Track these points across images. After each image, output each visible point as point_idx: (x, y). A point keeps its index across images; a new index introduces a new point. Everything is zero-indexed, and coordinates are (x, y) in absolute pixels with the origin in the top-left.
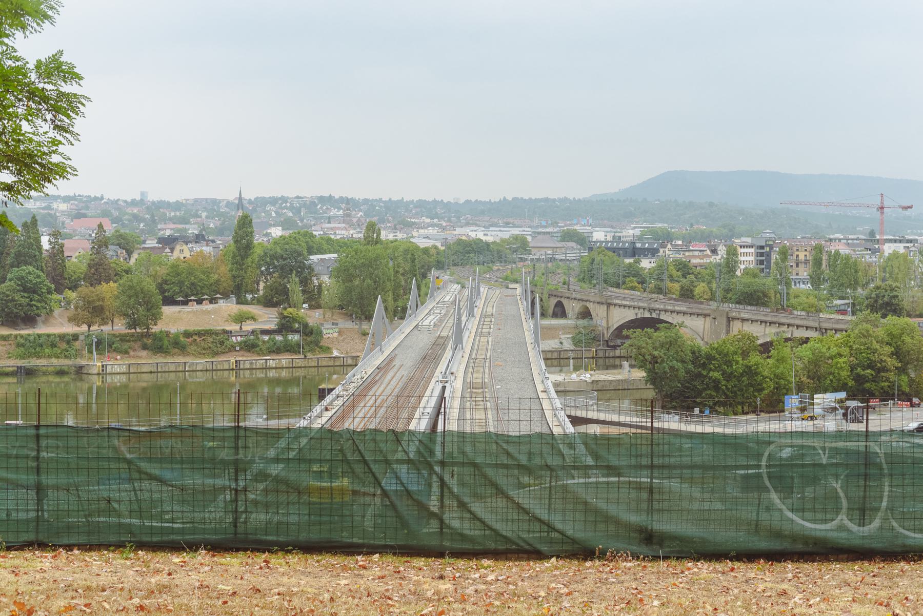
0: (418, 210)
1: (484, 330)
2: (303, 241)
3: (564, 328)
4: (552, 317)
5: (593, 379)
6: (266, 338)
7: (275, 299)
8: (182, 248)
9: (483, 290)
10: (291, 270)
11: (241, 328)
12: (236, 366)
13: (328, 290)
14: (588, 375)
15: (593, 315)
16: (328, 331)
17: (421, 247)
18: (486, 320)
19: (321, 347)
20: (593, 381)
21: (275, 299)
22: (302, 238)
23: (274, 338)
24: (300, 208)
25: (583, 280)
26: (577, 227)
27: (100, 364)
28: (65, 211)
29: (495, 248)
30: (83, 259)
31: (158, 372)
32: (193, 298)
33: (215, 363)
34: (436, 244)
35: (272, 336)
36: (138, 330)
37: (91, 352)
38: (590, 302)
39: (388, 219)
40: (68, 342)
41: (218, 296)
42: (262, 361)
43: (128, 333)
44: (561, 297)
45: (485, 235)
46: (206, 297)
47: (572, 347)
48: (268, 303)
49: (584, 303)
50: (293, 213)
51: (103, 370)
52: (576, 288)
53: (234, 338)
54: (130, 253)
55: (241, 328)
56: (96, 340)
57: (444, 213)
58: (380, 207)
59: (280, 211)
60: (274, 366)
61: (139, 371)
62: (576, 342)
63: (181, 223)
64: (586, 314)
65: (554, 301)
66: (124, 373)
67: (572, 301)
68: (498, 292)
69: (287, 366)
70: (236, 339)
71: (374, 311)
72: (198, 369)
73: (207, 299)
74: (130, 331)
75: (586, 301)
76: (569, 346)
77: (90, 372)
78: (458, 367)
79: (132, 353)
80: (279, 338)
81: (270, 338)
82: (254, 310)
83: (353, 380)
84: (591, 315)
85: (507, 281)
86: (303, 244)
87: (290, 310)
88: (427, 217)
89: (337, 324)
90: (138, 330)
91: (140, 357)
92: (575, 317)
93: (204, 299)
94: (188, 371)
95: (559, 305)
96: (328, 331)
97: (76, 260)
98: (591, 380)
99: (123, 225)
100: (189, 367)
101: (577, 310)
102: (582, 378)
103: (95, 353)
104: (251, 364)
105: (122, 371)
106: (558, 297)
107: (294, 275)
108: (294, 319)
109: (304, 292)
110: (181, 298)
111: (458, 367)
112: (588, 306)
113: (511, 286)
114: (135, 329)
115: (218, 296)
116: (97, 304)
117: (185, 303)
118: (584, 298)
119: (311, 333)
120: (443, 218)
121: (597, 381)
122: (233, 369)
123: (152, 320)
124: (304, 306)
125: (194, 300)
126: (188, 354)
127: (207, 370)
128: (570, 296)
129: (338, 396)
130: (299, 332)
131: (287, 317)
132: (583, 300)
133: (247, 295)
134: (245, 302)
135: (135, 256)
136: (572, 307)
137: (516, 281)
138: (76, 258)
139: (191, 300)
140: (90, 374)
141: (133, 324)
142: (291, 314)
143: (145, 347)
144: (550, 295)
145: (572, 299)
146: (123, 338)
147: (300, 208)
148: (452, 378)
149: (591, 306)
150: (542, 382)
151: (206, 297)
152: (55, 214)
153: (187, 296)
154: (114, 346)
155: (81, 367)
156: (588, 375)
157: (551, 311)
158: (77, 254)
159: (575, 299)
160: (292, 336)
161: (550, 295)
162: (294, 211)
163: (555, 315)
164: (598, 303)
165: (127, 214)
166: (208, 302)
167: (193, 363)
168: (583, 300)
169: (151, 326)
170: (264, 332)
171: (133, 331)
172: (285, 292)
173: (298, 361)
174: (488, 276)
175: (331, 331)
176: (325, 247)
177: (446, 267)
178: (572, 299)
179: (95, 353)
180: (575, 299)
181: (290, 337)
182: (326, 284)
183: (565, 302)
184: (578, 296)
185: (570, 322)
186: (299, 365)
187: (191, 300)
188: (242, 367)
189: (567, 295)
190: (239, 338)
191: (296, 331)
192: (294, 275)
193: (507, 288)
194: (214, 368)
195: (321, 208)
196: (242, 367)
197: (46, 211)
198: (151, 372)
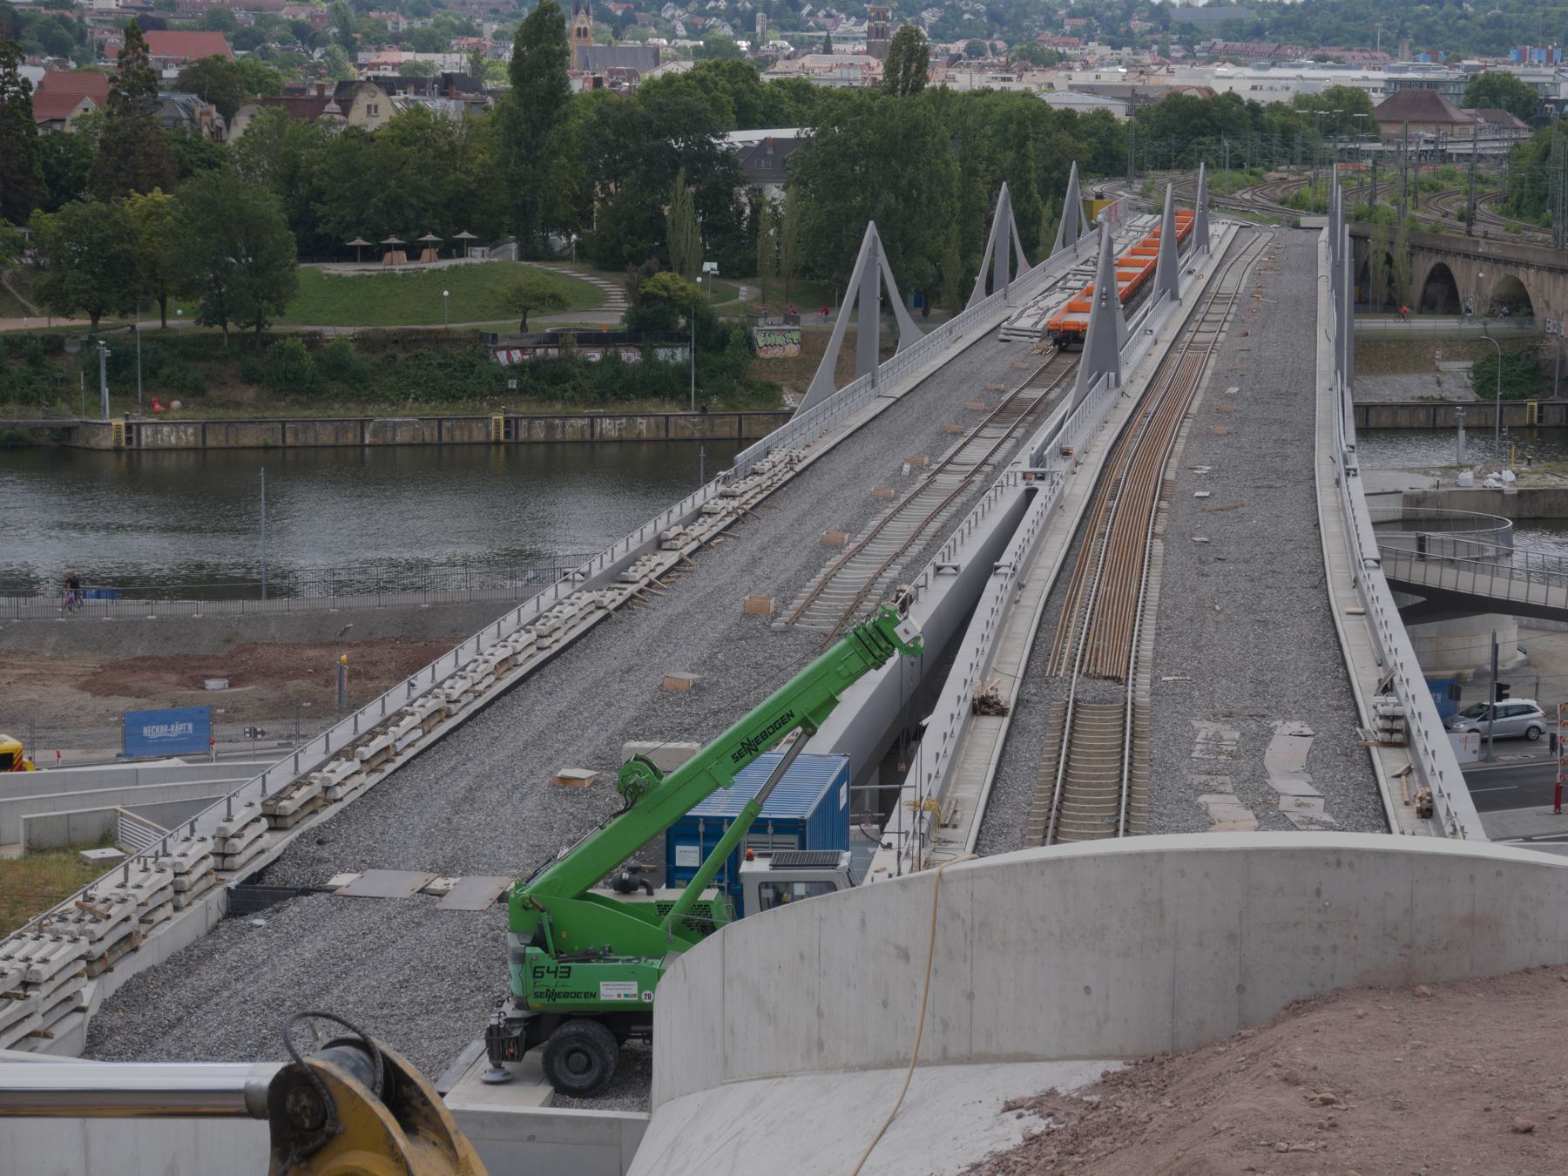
0: (1081, 22)
1: (1199, 337)
2: (724, 91)
3: (1453, 346)
4: (1420, 312)
5: (1524, 485)
6: (595, 356)
7: (626, 248)
8: (373, 102)
9: (1221, 230)
10: (676, 167)
11: (524, 326)
12: (507, 434)
13: (778, 223)
14: (1508, 475)
15: (1537, 303)
16: (771, 339)
17: (1056, 108)
18: (1214, 309)
19: (749, 386)
20: (1521, 493)
21: (626, 248)
22: (723, 82)
23: (618, 356)
24: (754, 11)
25: (1518, 210)
26: (1516, 70)
27: (122, 422)
28: (109, 12)
29: (1277, 119)
30: (95, 125)
31: (285, 447)
32: (393, 240)
33: (447, 424)
34: (1112, 109)
35: (611, 352)
36: (232, 327)
37: (94, 387)
38: (1528, 265)
39: (993, 48)
40: (34, 360)
41: (465, 235)
42: (580, 422)
43: (205, 336)
44: (1447, 253)
45: (1254, 88)
46: (430, 237)
47: (1472, 397)
48: (607, 258)
49: (1511, 271)
50: (734, 27)
51: (129, 440)
52: (1492, 230)
53: (502, 356)
54: (228, 113)
55: (524, 326)
56: (108, 353)
57: (1151, 32)
58: (976, 13)
59: (699, 21)
60: (614, 434)
61: (232, 443)
62: (1483, 381)
63: (422, 49)
64: (1516, 302)
65: (1425, 265)
66: (190, 449)
67: (1475, 265)
68: (1267, 236)
69: (652, 436)
70: (509, 356)
71: (854, 262)
72: (398, 439)
73: (434, 244)
74: (207, 330)
75: (1517, 264)
76: (1461, 392)
77: (93, 443)
78: (1093, 436)
79: (214, 393)
80: (630, 356)
81: (605, 358)
82: (571, 274)
83: (758, 467)
84: (1530, 306)
85: (1293, 208)
86: (725, 98)
87: (664, 276)
88: (1102, 42)
89: (796, 321)
90: (232, 327)
91: (238, 405)
92: (1484, 310)
93: (426, 245)
94: (369, 446)
95: (1441, 275)
96: (771, 339)
97: (73, 130)
98: (1514, 490)
99: (266, 54)
100: (375, 434)
101: (1489, 290)
102: (1491, 482)
103: (106, 391)
104: (550, 428)
105: (183, 443)
106: (1438, 251)
107: (680, 179)
108: (673, 303)
109: (707, 230)
110: (359, 242)
111: (1093, 436)
112: (1522, 277)
113: (1306, 221)
114: (224, 325)
115: (465, 235)
116: (116, 247)
117: (372, 254)
118: (1512, 255)
119: (723, 340)
120: (1146, 47)
121: (1532, 493)
122: (497, 443)
123: (271, 300)
124: (708, 266)
125: (398, 247)
126: (374, 399)
127: (424, 445)
128: (1471, 249)
129: (699, 513)
130: (688, 339)
131: (655, 297)
132: (1507, 262)
133: (552, 236)
134: (549, 256)
135: (241, 123)
136: (1478, 282)
137: (1320, 209)
138: (74, 123)
139: (389, 248)
140: (92, 450)
141: (215, 314)
142: (666, 288)
143: (250, 378)
144: (1415, 249)
145: (1477, 257)
146: (189, 349)
147: (754, 11)
148: (1062, 466)
149: (1529, 278)
150: (1338, 482)
151: (430, 237)
152: (81, 19)
153: (378, 235)
154: (165, 371)
155: (69, 430)
156: (1508, 475)
157: (1416, 292)
158: (78, 112)
159: (1487, 259)
160: (668, 352)
161: (1415, 249)
162: (737, 21)
163: (1428, 306)
164: (1551, 270)
165: (278, 22)
166: (434, 252)
167: (385, 425)
168: (1507, 262)
169: (268, 318)
170: (590, 338)
171: (218, 329)
172: (656, 228)
173: (682, 422)
174: (1247, 196)
175: (779, 340)
176: (788, 106)
177: (1131, 169)
178: (1477, 257)
179: (106, 391)
180: (1487, 259)
181: (662, 354)
182: (775, 208)
183: (1457, 267)
184: (1495, 251)
185: (1466, 325)
186: (687, 434)
187: (389, 248)
188: (523, 436)
189: (1462, 247)
190: (517, 356)
191: (680, 338)
192: (680, 179)
193: (1297, 226)
194: (445, 438)
195: (810, 14)
196: (523, 436)
197: (55, 12)
198: (266, 448)
